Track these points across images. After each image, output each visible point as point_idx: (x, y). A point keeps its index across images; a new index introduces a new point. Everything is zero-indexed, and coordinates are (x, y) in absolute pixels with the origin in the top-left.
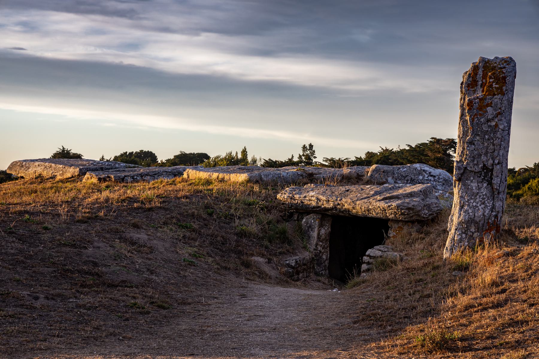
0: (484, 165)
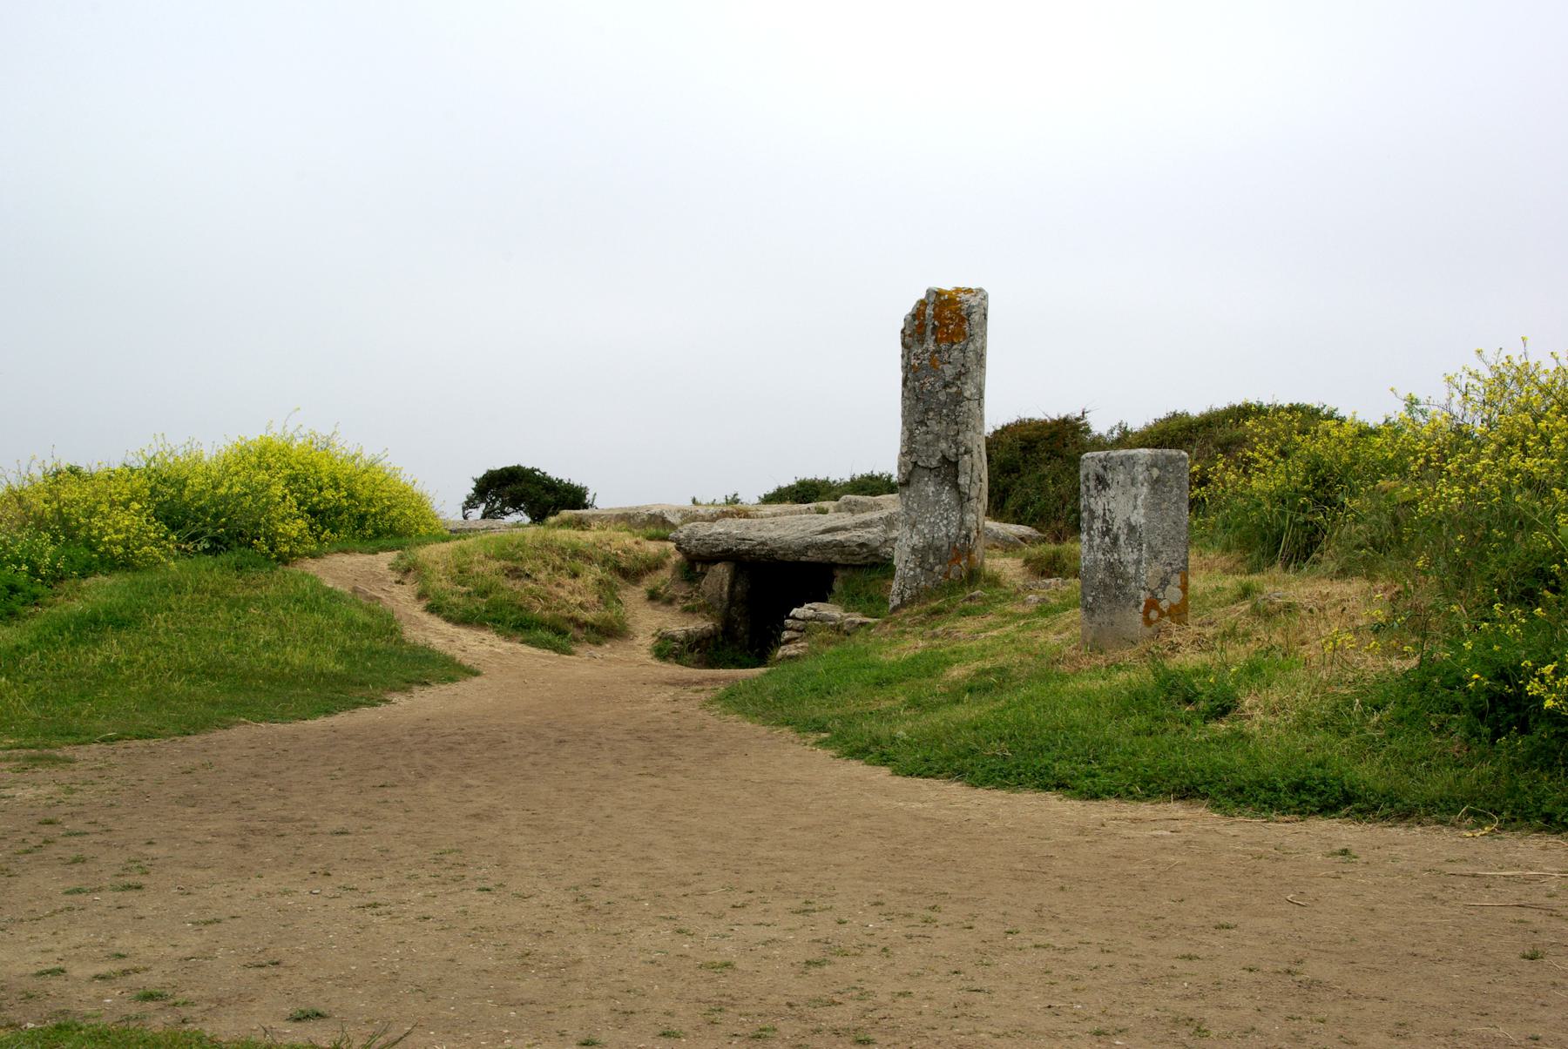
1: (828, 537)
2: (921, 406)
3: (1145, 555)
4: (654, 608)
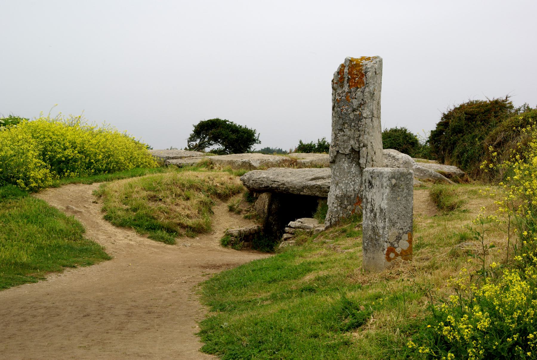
0: (352, 148)
1: (313, 183)
2: (341, 121)
3: (387, 224)
4: (231, 216)
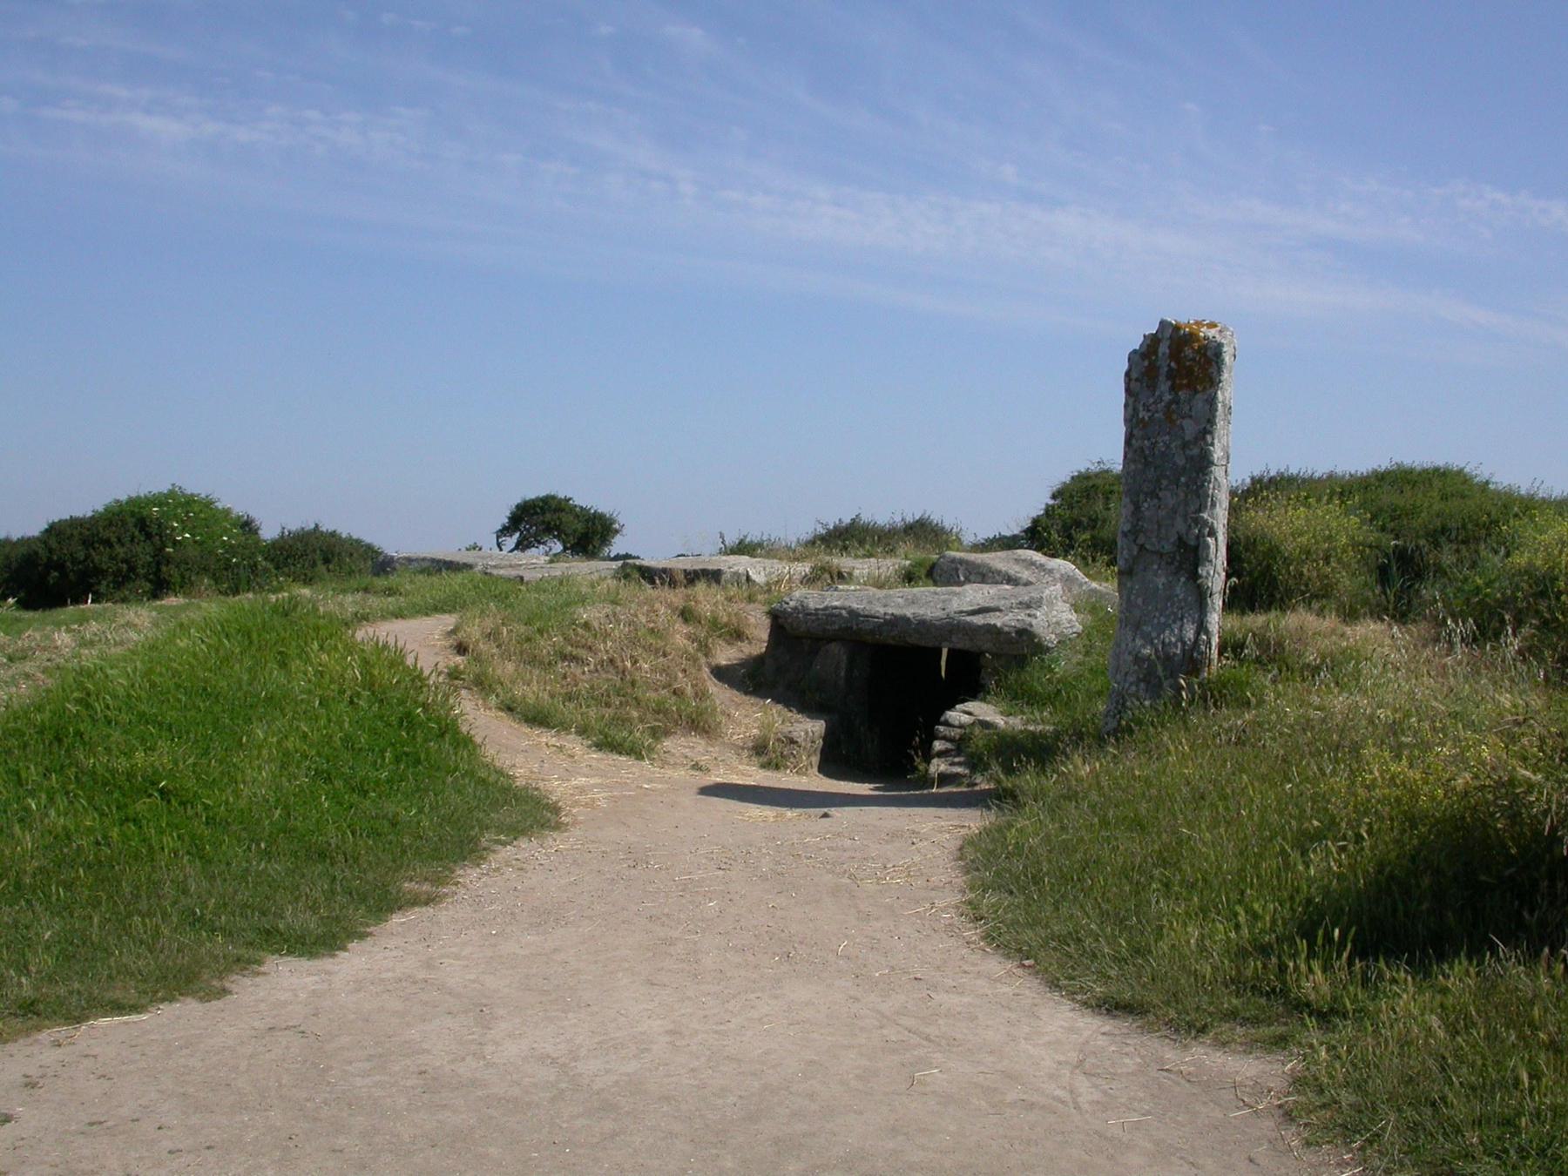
0: (1180, 539)
1: (978, 620)
